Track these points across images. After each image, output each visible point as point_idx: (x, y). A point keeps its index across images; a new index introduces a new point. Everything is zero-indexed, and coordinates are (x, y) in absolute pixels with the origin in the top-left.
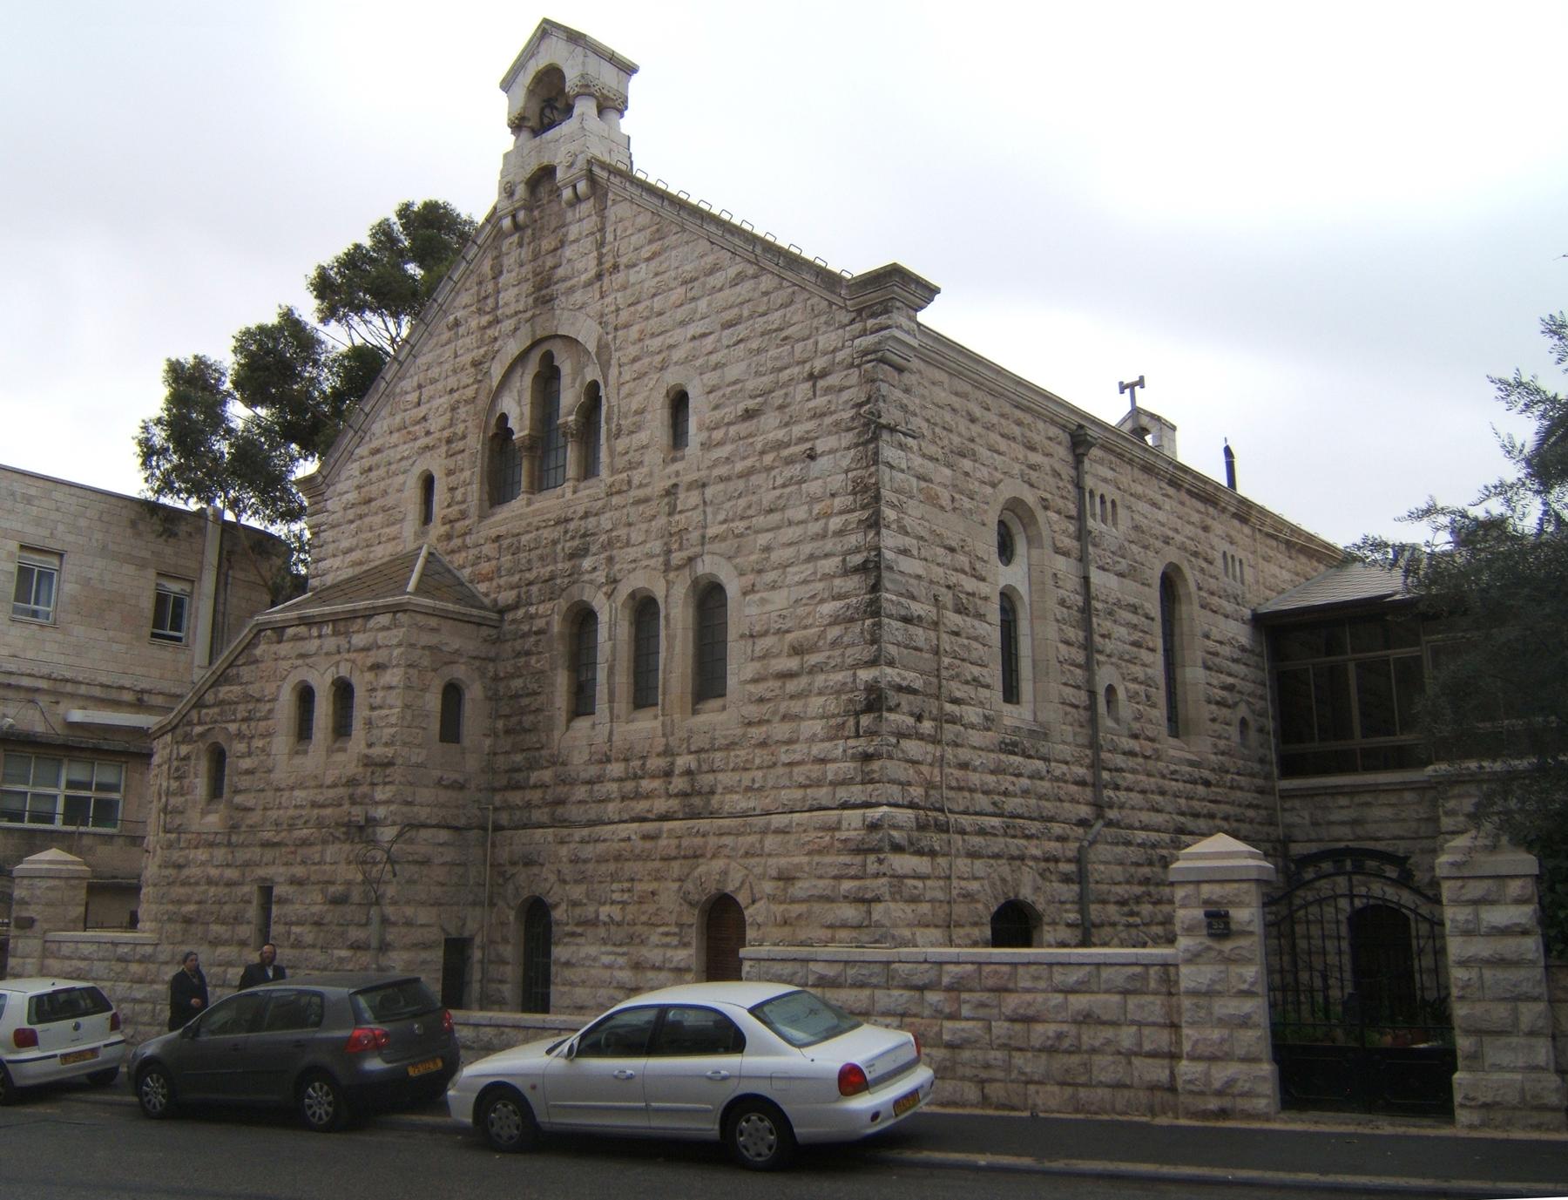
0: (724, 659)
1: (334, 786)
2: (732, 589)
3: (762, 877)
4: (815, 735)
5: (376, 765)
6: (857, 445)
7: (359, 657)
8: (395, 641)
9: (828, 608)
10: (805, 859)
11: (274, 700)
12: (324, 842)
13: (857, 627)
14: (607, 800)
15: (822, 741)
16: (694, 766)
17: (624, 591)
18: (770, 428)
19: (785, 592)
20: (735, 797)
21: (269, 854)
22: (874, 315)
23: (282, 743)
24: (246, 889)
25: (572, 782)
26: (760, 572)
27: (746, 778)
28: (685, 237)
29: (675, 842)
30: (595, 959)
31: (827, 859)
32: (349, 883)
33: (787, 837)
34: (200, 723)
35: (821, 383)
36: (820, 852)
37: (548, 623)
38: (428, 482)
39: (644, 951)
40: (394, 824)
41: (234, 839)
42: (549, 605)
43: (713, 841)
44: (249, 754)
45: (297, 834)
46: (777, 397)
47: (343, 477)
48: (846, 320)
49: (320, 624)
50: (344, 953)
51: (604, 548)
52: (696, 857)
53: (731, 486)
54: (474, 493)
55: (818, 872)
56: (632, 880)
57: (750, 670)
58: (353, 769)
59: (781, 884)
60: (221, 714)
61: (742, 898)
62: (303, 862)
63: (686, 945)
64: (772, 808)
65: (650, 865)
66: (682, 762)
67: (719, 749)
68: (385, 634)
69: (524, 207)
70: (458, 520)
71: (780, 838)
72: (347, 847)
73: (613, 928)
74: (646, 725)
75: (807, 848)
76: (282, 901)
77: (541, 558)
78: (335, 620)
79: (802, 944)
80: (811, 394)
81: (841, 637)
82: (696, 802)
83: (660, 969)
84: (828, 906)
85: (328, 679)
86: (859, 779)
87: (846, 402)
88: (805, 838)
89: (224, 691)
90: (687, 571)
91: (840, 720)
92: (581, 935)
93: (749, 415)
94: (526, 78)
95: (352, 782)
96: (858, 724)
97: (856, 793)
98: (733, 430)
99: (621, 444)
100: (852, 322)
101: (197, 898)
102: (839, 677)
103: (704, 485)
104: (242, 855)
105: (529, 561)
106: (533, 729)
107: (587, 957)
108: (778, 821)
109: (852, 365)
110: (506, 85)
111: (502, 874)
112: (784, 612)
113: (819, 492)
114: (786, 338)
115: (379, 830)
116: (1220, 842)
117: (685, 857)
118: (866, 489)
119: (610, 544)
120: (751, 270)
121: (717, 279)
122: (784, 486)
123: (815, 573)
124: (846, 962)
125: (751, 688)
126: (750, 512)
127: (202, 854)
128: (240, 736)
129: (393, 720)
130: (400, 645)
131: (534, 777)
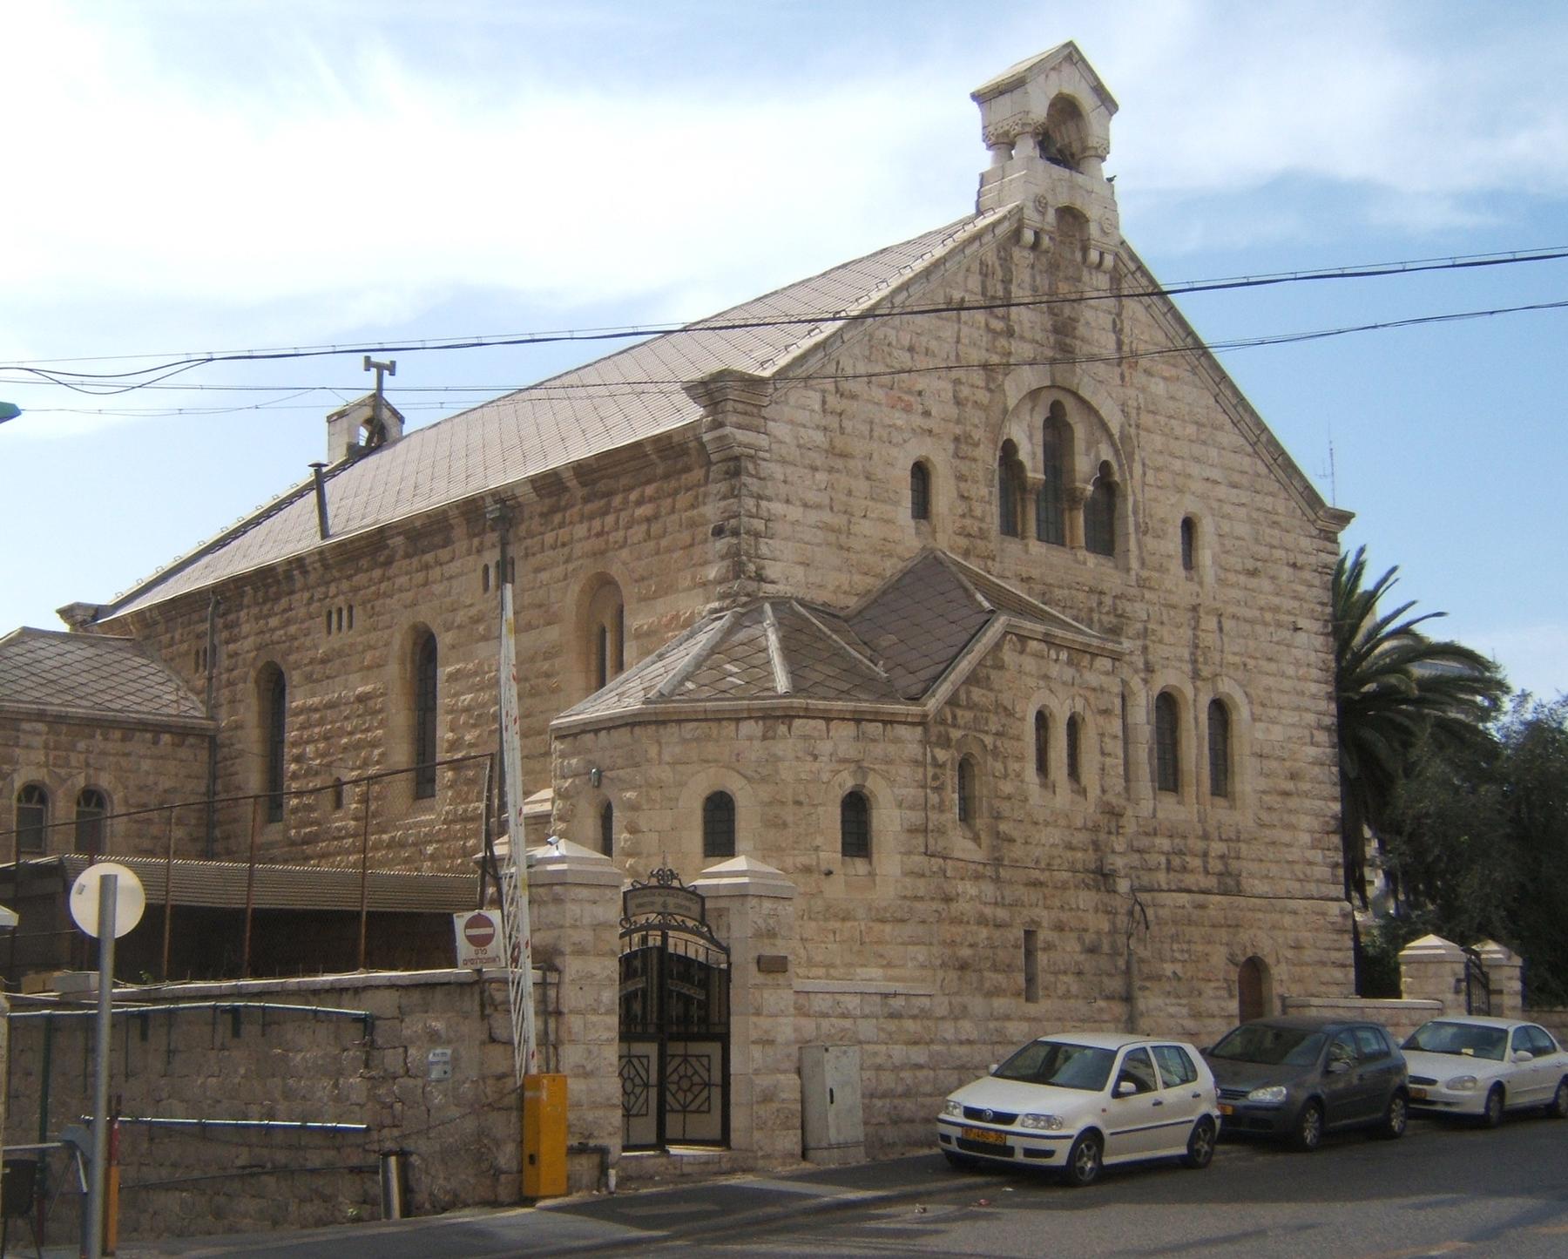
38: (921, 472)
49: (1059, 647)
51: (1138, 636)
57: (1263, 784)
61: (1270, 960)
76: (1049, 947)
82: (1230, 884)
95: (1096, 829)
104: (1009, 894)
116: (1431, 940)
120: (1249, 449)
122: (1278, 643)
127: (970, 889)
128: (995, 753)
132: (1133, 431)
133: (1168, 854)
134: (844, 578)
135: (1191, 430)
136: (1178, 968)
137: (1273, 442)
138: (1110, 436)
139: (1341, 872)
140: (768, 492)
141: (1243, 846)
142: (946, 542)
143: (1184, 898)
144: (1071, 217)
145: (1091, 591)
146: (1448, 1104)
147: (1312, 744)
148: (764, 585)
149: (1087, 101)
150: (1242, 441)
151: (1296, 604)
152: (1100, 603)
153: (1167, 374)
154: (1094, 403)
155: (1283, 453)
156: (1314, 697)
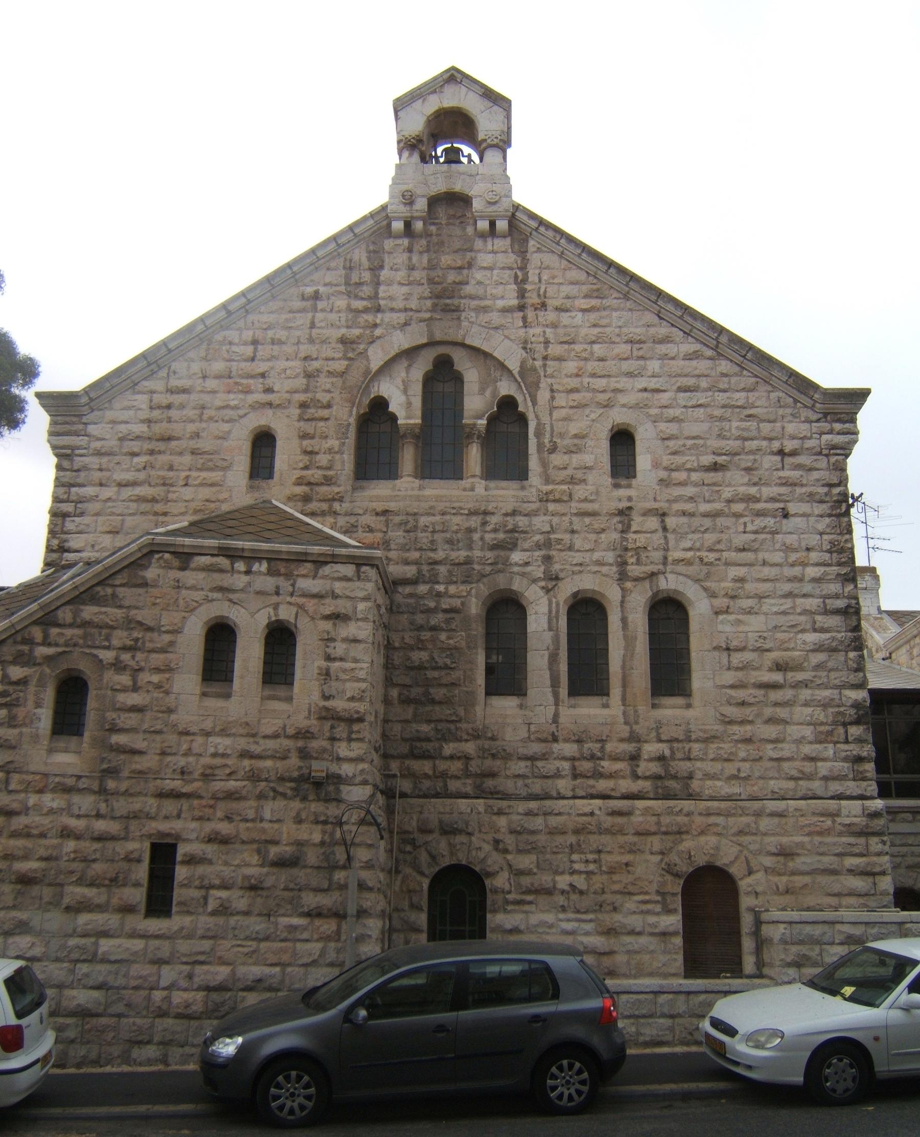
0: (233, 661)
1: (276, 736)
2: (699, 608)
3: (759, 852)
4: (803, 737)
5: (340, 719)
6: (830, 515)
7: (310, 604)
8: (361, 594)
9: (812, 638)
10: (806, 839)
11: (176, 632)
12: (261, 796)
13: (841, 657)
14: (557, 775)
15: (811, 743)
16: (667, 753)
17: (566, 590)
18: (736, 482)
19: (761, 618)
20: (719, 783)
21: (170, 806)
22: (839, 421)
23: (188, 681)
24: (131, 846)
25: (507, 757)
26: (733, 597)
27: (730, 769)
28: (629, 304)
29: (654, 819)
30: (551, 926)
31: (829, 840)
32: (299, 844)
33: (784, 820)
34: (46, 643)
35: (789, 460)
36: (820, 833)
37: (463, 604)
38: (264, 442)
39: (618, 917)
40: (365, 783)
41: (111, 784)
42: (463, 588)
43: (699, 820)
44: (135, 688)
45: (217, 786)
46: (746, 460)
47: (117, 405)
48: (815, 417)
50: (296, 921)
52: (680, 833)
53: (696, 521)
54: (346, 463)
55: (821, 850)
56: (599, 852)
58: (301, 721)
59: (781, 859)
60: (85, 637)
62: (228, 818)
63: (669, 911)
64: (760, 795)
65: (621, 839)
66: (651, 748)
67: (697, 741)
68: (344, 584)
69: (423, 219)
70: (322, 484)
71: (776, 820)
72: (296, 805)
73: (574, 897)
74: (588, 712)
75: (807, 830)
77: (450, 542)
78: (273, 559)
79: (808, 909)
80: (780, 466)
81: (826, 662)
82: (670, 784)
83: (639, 934)
84: (832, 878)
85: (262, 619)
86: (851, 776)
87: (818, 480)
88: (803, 821)
89: (89, 612)
90: (647, 584)
91: (827, 728)
92: (530, 903)
93: (715, 467)
94: (433, 105)
95: (304, 734)
96: (846, 732)
97: (852, 787)
98: (695, 476)
99: (557, 459)
101: (43, 852)
102: (827, 693)
103: (664, 514)
104: (122, 806)
105: (432, 542)
106: (447, 702)
107: (543, 923)
108: (772, 806)
109: (820, 453)
110: (401, 105)
111: (413, 842)
112: (765, 635)
113: (796, 545)
114: (750, 416)
115: (345, 789)
117: (666, 833)
118: (841, 551)
119: (548, 544)
121: (671, 349)
123: (793, 608)
124: (866, 923)
125: (732, 692)
126: (718, 547)
128: (118, 666)
129: (362, 674)
130: (365, 599)
131: (449, 748)
132: (538, 363)
133: (573, 759)
134: (812, 638)
135: (624, 349)
137: (737, 341)
138: (509, 372)
139: (870, 767)
141: (696, 746)
142: (279, 493)
144: (454, 202)
145: (472, 513)
146: (749, 1067)
148: (66, 554)
149: (472, 104)
150: (698, 346)
151: (783, 490)
152: (484, 523)
154: (485, 347)
155: (751, 347)
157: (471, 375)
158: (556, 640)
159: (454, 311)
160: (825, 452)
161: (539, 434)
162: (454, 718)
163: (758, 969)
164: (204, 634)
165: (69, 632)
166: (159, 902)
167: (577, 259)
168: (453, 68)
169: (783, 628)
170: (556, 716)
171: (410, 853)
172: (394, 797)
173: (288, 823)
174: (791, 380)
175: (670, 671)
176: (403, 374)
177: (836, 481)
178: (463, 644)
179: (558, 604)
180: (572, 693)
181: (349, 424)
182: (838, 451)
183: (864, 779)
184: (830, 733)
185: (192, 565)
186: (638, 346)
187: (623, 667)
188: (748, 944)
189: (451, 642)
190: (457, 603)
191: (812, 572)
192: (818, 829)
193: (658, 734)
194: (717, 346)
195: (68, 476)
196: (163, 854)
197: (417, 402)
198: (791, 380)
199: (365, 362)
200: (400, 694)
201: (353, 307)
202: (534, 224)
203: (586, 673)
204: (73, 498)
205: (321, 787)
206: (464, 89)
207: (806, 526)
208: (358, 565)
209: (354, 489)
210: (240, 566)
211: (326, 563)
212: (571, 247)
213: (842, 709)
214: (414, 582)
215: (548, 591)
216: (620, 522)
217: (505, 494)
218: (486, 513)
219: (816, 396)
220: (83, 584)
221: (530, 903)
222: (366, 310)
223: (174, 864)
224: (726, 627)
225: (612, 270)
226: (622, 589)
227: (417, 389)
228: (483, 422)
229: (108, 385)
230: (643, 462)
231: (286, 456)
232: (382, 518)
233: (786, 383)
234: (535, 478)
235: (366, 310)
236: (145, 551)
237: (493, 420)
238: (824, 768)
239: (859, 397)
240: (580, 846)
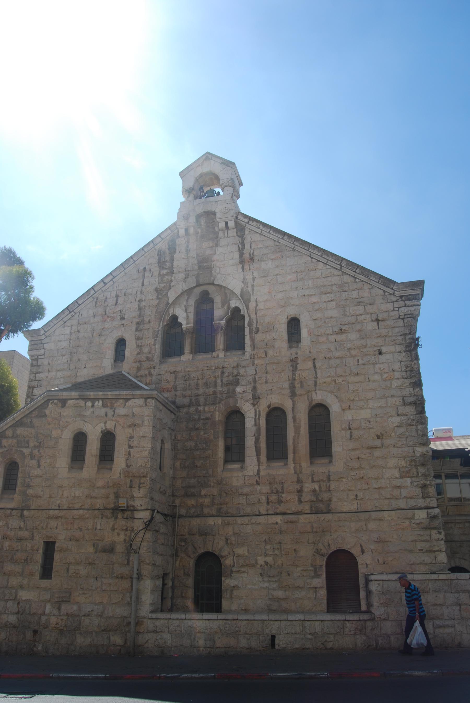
2: (335, 408)
19: (369, 411)
22: (409, 299)
23: (63, 462)
37: (211, 415)
38: (121, 343)
42: (212, 408)
61: (355, 552)
72: (111, 522)
74: (278, 470)
80: (377, 327)
82: (321, 506)
89: (19, 431)
91: (407, 469)
92: (244, 572)
97: (421, 503)
100: (397, 301)
111: (185, 541)
128: (32, 456)
132: (250, 289)
136: (269, 559)
140: (40, 370)
143: (279, 519)
147: (398, 415)
151: (380, 340)
153: (273, 257)
155: (358, 266)
156: (399, 388)
157: (218, 300)
158: (259, 430)
159: (208, 268)
160: (401, 317)
161: (250, 324)
162: (207, 475)
163: (368, 608)
164: (72, 437)
165: (10, 441)
166: (47, 572)
167: (268, 234)
168: (208, 153)
169: (381, 415)
170: (259, 471)
171: (184, 546)
172: (175, 517)
173: (111, 532)
174: (380, 281)
175: (321, 445)
176: (185, 303)
177: (408, 332)
178: (212, 437)
179: (259, 412)
180: (270, 458)
181: (159, 330)
182: (409, 316)
183: (428, 497)
184: (408, 472)
185: (67, 405)
186: (300, 274)
187: (294, 443)
188: (363, 594)
189: (206, 435)
190: (209, 415)
191: (395, 383)
192: (401, 527)
193: (312, 478)
194: (341, 268)
195: (35, 369)
196: (49, 547)
197: (192, 316)
198: (380, 281)
199: (167, 299)
200: (181, 464)
201: (161, 273)
202: (246, 220)
203: (276, 447)
204: (37, 379)
205: (126, 511)
206: (213, 162)
207: (393, 357)
208: (146, 399)
209: (161, 363)
210: (89, 404)
211: (130, 399)
212: (265, 229)
213: (414, 458)
214: (189, 406)
215: (254, 405)
216: (291, 366)
217: (233, 358)
218: (223, 368)
219: (395, 288)
220: (17, 417)
221: (244, 572)
222: (167, 274)
223: (54, 552)
224: (349, 416)
225: (285, 237)
226: (293, 401)
227: (191, 309)
228: (223, 322)
229: (52, 324)
230: (304, 333)
231: (130, 351)
232: (173, 375)
233: (378, 282)
234: (248, 348)
235: (167, 274)
236: (45, 399)
237: (229, 321)
238: (404, 493)
239: (420, 284)
240: (270, 541)
